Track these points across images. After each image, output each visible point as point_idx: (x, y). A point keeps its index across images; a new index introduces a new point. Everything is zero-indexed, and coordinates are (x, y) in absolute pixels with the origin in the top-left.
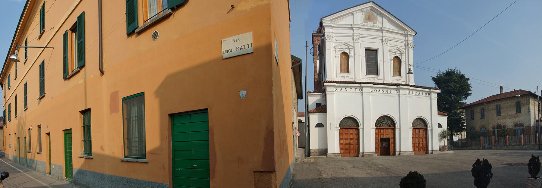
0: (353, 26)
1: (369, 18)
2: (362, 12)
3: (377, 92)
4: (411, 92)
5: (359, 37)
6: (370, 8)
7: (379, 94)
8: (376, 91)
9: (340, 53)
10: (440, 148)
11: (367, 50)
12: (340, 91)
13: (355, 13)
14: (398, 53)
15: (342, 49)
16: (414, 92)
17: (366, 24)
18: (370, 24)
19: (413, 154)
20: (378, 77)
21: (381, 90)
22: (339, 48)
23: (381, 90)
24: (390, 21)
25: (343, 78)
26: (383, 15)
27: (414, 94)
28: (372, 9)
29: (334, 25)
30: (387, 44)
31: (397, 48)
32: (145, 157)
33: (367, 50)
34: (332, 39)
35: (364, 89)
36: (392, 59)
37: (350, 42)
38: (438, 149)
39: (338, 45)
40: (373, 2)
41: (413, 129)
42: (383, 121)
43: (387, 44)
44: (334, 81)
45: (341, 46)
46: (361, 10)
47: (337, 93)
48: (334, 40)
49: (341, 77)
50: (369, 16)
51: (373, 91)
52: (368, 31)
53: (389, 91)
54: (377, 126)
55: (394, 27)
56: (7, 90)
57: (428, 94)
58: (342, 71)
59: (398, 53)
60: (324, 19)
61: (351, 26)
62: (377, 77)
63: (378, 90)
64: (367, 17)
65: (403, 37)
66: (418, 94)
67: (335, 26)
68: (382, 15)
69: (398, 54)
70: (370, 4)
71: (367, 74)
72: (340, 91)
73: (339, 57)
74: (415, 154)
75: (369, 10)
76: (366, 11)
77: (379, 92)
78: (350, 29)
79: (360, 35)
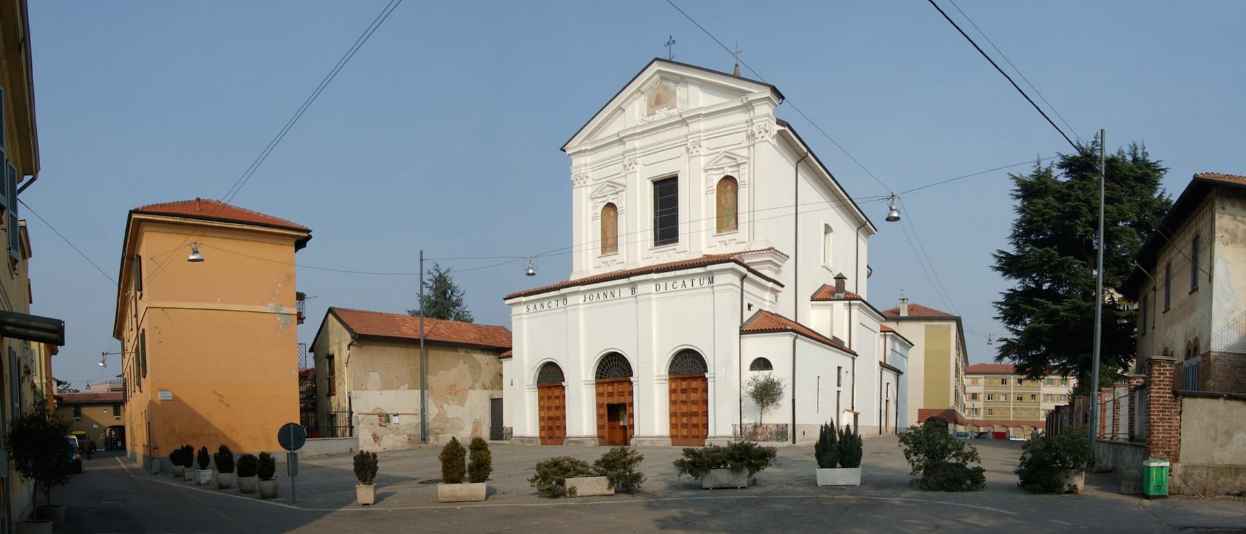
0: (684, 116)
1: (658, 102)
2: (643, 93)
4: (546, 304)
5: (635, 158)
6: (657, 75)
7: (599, 304)
9: (717, 179)
13: (627, 106)
14: (730, 167)
15: (721, 171)
16: (670, 284)
18: (662, 114)
22: (715, 167)
24: (704, 85)
25: (723, 245)
26: (687, 79)
27: (670, 288)
28: (664, 77)
29: (586, 148)
30: (698, 153)
31: (726, 152)
34: (585, 179)
35: (569, 298)
37: (620, 175)
39: (710, 162)
40: (656, 59)
42: (694, 360)
43: (698, 153)
46: (638, 90)
47: (658, 296)
48: (589, 182)
49: (602, 265)
50: (658, 95)
52: (656, 136)
54: (601, 378)
55: (719, 98)
56: (142, 379)
57: (706, 281)
59: (730, 167)
60: (567, 146)
61: (679, 119)
64: (654, 100)
65: (742, 114)
66: (679, 288)
67: (589, 148)
68: (683, 80)
69: (730, 170)
70: (656, 67)
71: (656, 244)
73: (600, 218)
75: (657, 83)
76: (651, 88)
77: (684, 287)
78: (620, 145)
79: (638, 152)
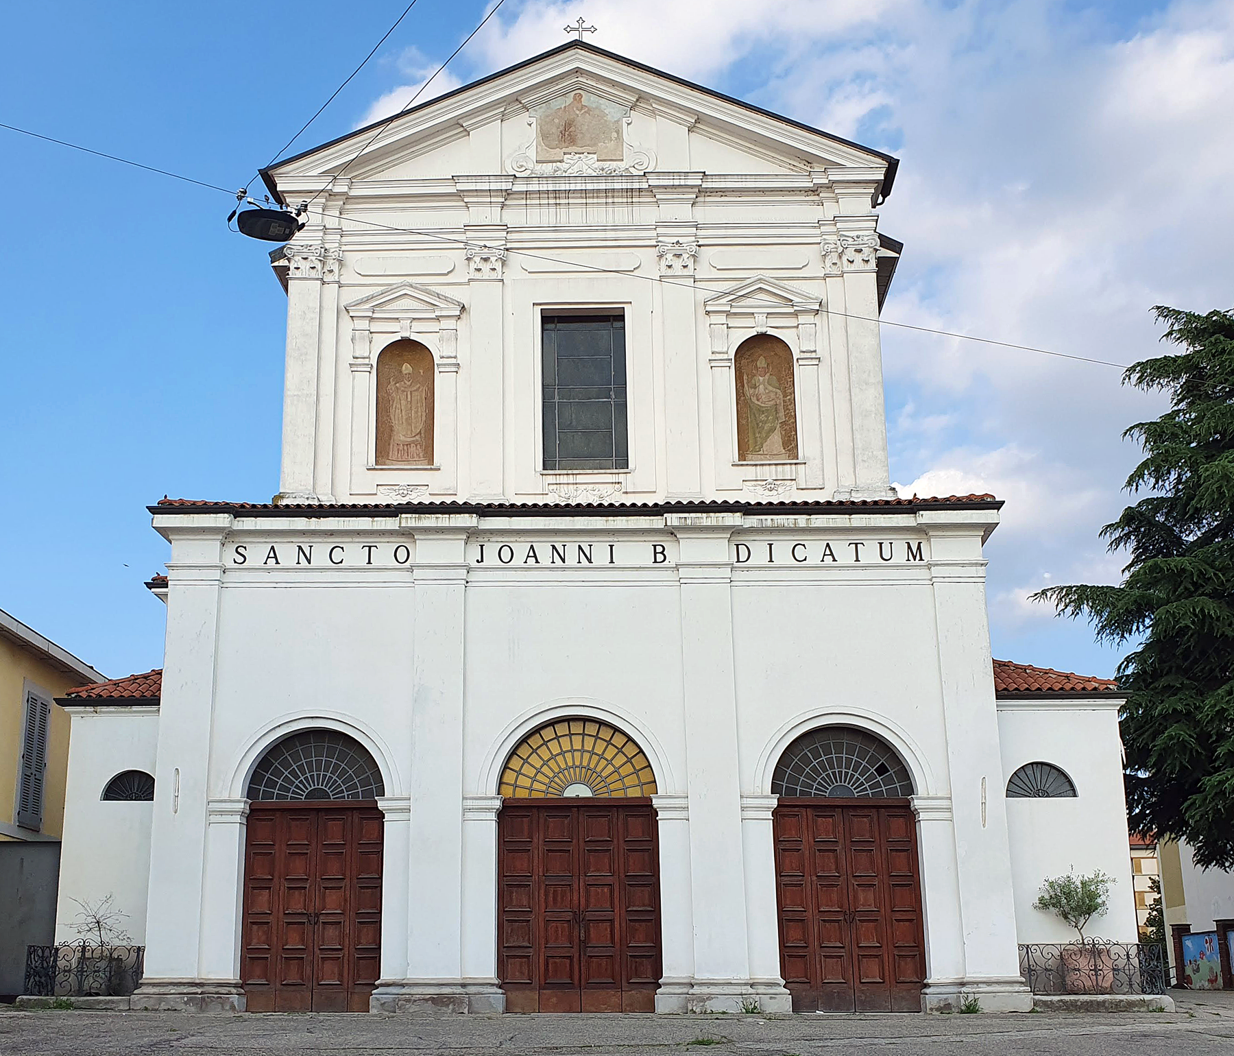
3: (518, 561)
4: (521, 549)
8: (506, 554)
10: (1029, 971)
11: (552, 319)
12: (904, 561)
17: (548, 169)
18: (583, 164)
19: (782, 1002)
20: (621, 478)
21: (544, 551)
23: (544, 551)
32: (251, 785)
33: (552, 319)
36: (732, 355)
38: (1015, 973)
41: (779, 815)
44: (182, 502)
45: (388, 307)
51: (491, 559)
53: (600, 553)
58: (393, 454)
62: (614, 478)
63: (521, 549)
72: (904, 561)
74: (796, 1007)
